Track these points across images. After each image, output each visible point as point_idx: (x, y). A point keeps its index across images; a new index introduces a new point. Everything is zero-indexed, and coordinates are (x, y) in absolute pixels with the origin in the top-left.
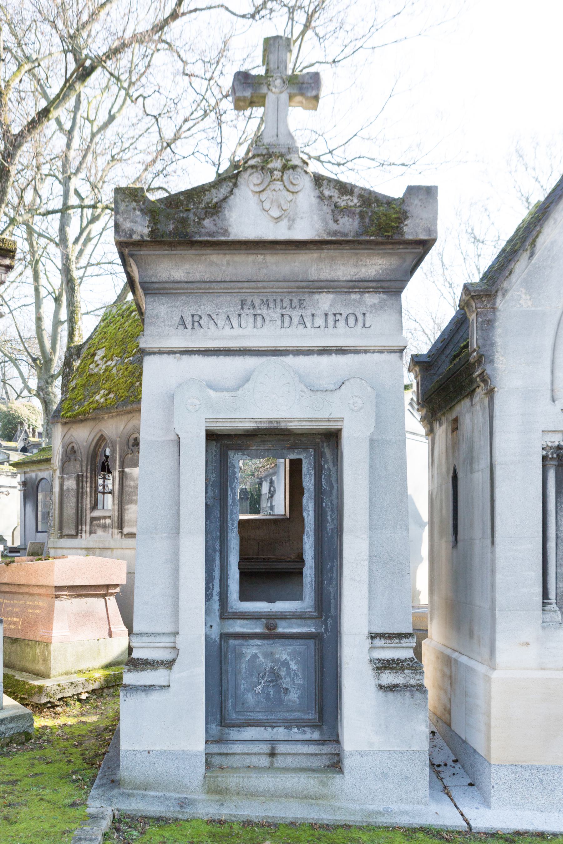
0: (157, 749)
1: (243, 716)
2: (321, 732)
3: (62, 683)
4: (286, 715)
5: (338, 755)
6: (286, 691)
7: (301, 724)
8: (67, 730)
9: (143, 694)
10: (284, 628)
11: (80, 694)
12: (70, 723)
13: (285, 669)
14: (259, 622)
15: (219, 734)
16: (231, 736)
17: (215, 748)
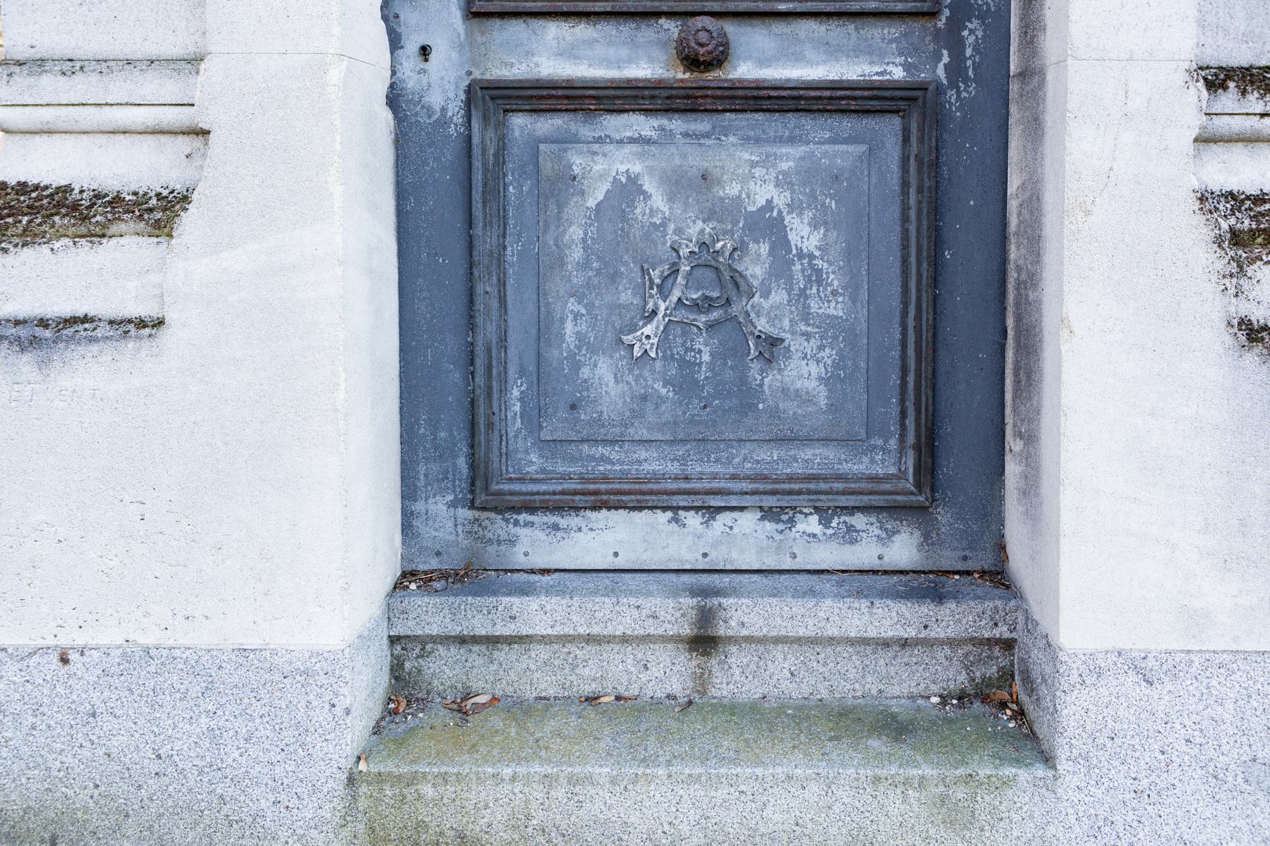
0: (104, 640)
1: (573, 460)
2: (926, 536)
4: (768, 457)
5: (1008, 645)
6: (771, 347)
7: (835, 500)
10: (762, 62)
13: (764, 249)
14: (647, 32)
15: (465, 542)
16: (519, 549)
17: (431, 614)
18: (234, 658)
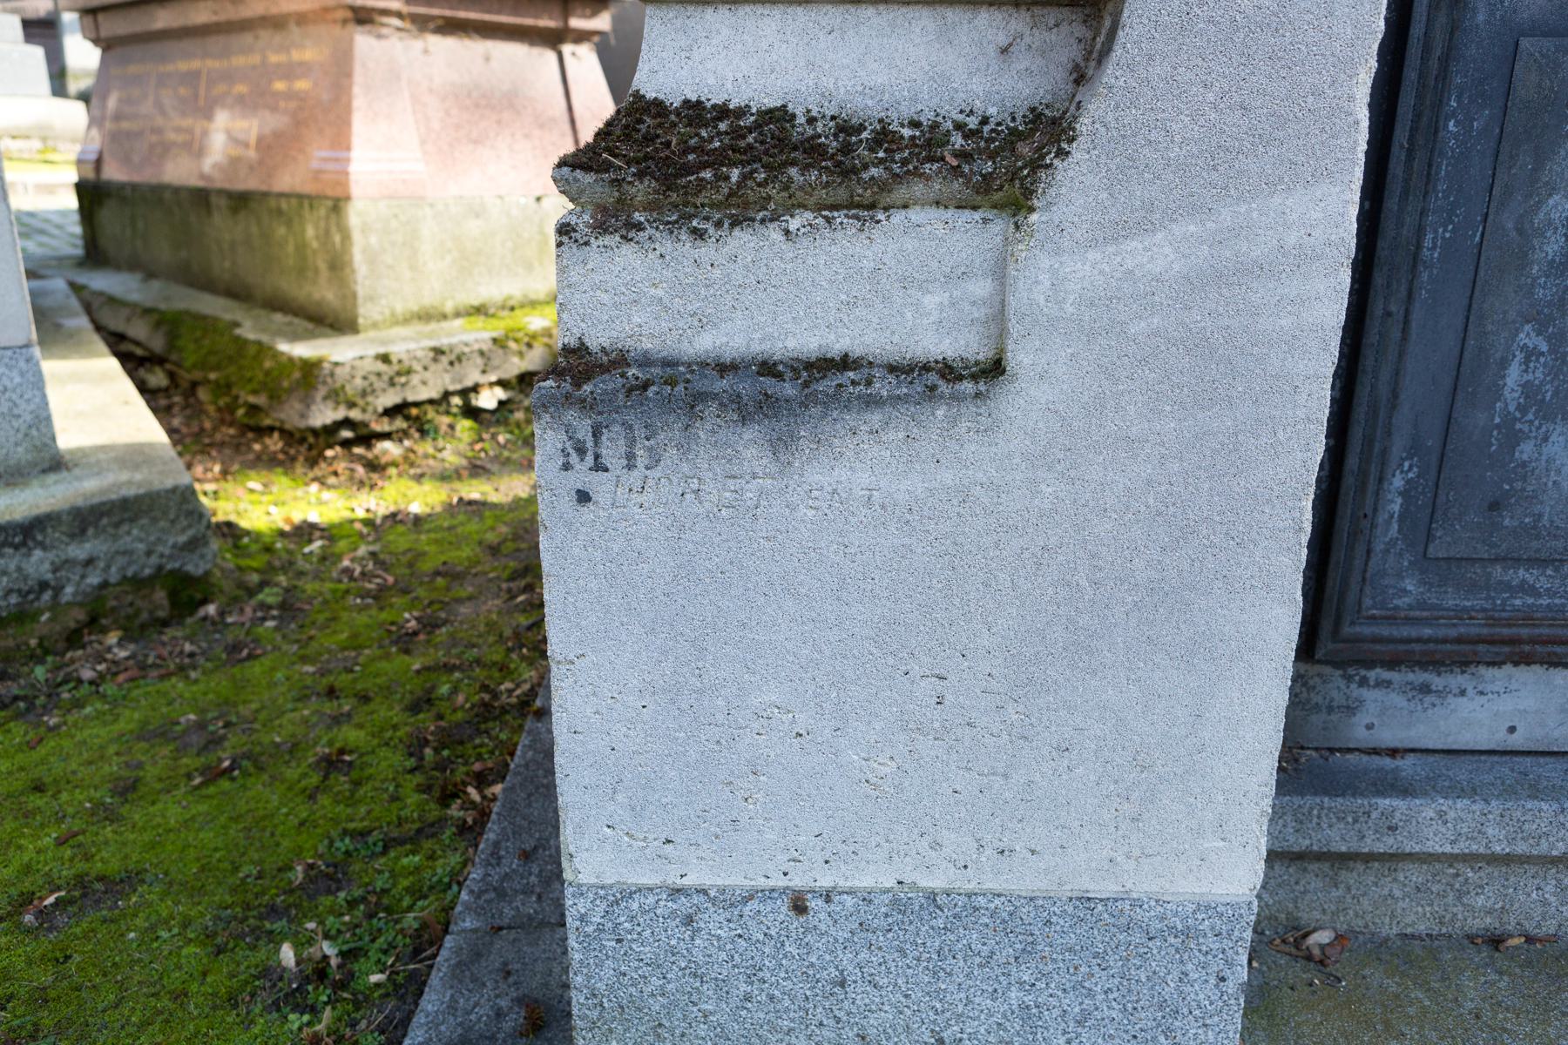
0: (865, 881)
3: (397, 350)
8: (400, 540)
9: (750, 446)
11: (475, 389)
12: (416, 508)
16: (1361, 719)
18: (1070, 910)
